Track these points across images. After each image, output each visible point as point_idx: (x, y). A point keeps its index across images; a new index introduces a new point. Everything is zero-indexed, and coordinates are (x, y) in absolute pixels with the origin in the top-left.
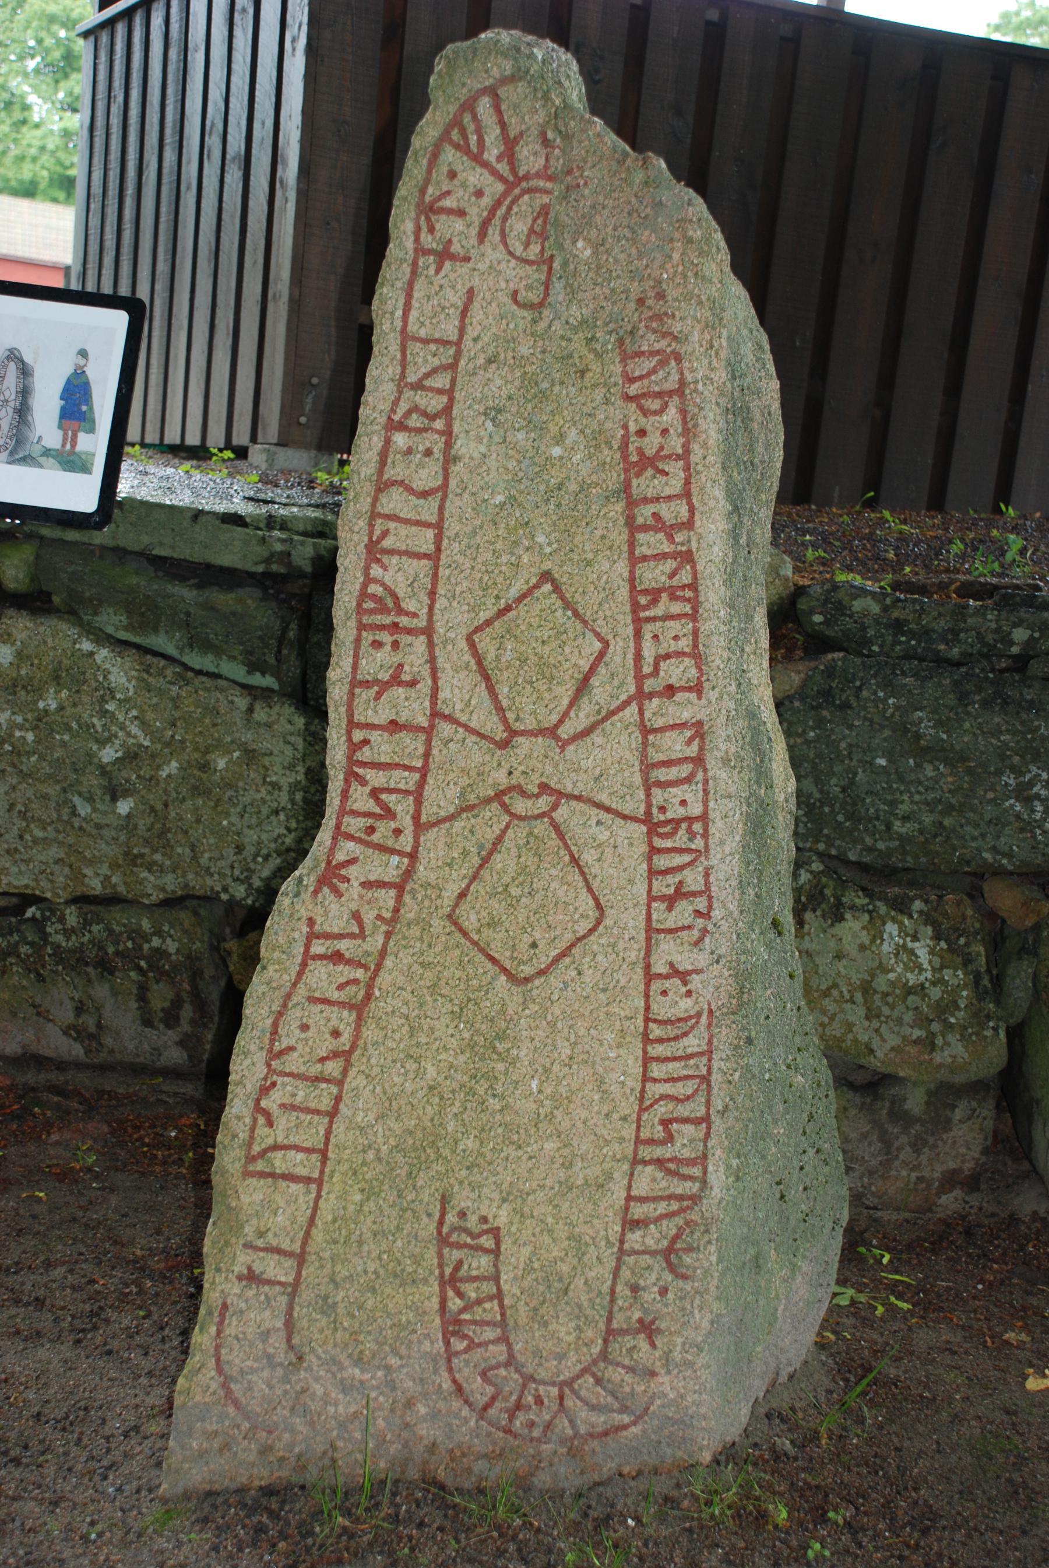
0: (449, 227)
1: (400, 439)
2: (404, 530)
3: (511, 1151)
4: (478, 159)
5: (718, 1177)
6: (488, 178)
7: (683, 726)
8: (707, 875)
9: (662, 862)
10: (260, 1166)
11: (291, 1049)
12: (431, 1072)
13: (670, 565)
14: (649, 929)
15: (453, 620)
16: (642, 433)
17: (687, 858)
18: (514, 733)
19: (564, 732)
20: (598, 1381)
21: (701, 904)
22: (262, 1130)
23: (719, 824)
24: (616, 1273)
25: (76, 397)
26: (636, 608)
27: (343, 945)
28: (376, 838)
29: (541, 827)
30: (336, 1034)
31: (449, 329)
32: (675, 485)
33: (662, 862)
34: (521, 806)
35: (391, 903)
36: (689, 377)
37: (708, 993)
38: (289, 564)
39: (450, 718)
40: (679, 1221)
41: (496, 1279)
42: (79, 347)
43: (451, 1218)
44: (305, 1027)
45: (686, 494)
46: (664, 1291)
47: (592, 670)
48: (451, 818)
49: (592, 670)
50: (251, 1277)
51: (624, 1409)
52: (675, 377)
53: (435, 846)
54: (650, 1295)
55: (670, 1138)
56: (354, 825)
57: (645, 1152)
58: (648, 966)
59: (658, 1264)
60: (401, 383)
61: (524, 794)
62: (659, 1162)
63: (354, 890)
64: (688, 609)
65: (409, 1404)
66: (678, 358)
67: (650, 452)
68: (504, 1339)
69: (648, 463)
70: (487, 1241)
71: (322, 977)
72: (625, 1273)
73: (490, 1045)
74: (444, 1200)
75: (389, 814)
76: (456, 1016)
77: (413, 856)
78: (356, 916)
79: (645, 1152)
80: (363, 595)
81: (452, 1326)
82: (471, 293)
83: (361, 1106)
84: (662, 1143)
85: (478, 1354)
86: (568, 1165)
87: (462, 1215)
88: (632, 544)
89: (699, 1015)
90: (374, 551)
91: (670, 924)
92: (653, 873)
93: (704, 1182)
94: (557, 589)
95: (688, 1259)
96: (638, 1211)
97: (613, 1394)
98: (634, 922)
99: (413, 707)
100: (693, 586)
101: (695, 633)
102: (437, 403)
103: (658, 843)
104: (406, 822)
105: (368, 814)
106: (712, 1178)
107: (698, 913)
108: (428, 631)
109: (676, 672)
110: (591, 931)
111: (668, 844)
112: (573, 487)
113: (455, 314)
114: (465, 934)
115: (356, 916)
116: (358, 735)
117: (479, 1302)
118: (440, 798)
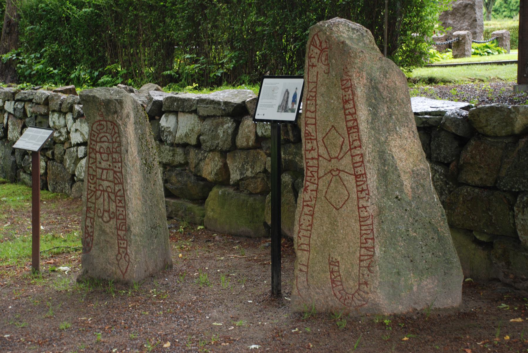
0: (314, 61)
1: (308, 102)
2: (310, 120)
3: (339, 245)
4: (316, 47)
5: (377, 251)
6: (318, 50)
7: (359, 155)
8: (367, 186)
9: (358, 183)
10: (300, 248)
11: (302, 224)
12: (325, 229)
13: (353, 121)
14: (358, 198)
15: (320, 137)
16: (345, 96)
17: (362, 182)
18: (331, 158)
19: (340, 157)
20: (359, 294)
21: (367, 192)
22: (299, 241)
23: (369, 175)
24: (359, 271)
25: (295, 96)
26: (348, 131)
27: (308, 203)
28: (312, 181)
29: (337, 177)
30: (309, 221)
31: (315, 80)
32: (352, 106)
33: (358, 183)
34: (334, 173)
35: (315, 194)
36: (353, 83)
37: (371, 211)
38: (428, 124)
39: (321, 156)
40: (370, 260)
41: (339, 272)
42: (287, 88)
43: (331, 259)
44: (304, 220)
45: (354, 107)
46: (368, 275)
47: (342, 145)
48: (323, 176)
49: (342, 145)
50: (301, 270)
51: (364, 301)
52: (350, 84)
53: (321, 183)
54: (366, 276)
55: (367, 242)
56: (308, 178)
57: (363, 245)
58: (358, 206)
59: (366, 269)
60: (308, 91)
61: (334, 171)
62: (365, 248)
63: (309, 191)
64: (356, 130)
65: (327, 297)
66: (351, 80)
67: (347, 99)
68: (342, 285)
69: (347, 102)
70: (337, 264)
71: (306, 209)
72: (361, 271)
73: (333, 223)
74: (329, 255)
75: (314, 176)
76: (328, 217)
77: (318, 184)
78: (310, 197)
79: (363, 245)
80: (305, 133)
81: (333, 282)
82: (318, 72)
83: (314, 237)
84: (365, 243)
85: (337, 287)
86: (349, 248)
87: (332, 258)
88: (346, 118)
89: (370, 216)
90: (306, 125)
91: (362, 196)
92: (357, 186)
93: (374, 252)
94: (335, 129)
95: (372, 269)
96: (362, 258)
97: (361, 297)
98: (355, 196)
99: (314, 154)
100: (357, 126)
101: (358, 135)
102: (313, 94)
103: (358, 179)
104: (316, 177)
105: (310, 176)
106: (376, 252)
107: (366, 194)
108: (316, 139)
109: (357, 143)
110: (348, 199)
111: (359, 180)
112: (335, 108)
113: (315, 76)
114: (327, 200)
115: (310, 197)
116: (307, 161)
117: (337, 277)
118: (321, 173)
